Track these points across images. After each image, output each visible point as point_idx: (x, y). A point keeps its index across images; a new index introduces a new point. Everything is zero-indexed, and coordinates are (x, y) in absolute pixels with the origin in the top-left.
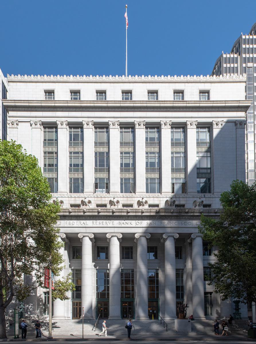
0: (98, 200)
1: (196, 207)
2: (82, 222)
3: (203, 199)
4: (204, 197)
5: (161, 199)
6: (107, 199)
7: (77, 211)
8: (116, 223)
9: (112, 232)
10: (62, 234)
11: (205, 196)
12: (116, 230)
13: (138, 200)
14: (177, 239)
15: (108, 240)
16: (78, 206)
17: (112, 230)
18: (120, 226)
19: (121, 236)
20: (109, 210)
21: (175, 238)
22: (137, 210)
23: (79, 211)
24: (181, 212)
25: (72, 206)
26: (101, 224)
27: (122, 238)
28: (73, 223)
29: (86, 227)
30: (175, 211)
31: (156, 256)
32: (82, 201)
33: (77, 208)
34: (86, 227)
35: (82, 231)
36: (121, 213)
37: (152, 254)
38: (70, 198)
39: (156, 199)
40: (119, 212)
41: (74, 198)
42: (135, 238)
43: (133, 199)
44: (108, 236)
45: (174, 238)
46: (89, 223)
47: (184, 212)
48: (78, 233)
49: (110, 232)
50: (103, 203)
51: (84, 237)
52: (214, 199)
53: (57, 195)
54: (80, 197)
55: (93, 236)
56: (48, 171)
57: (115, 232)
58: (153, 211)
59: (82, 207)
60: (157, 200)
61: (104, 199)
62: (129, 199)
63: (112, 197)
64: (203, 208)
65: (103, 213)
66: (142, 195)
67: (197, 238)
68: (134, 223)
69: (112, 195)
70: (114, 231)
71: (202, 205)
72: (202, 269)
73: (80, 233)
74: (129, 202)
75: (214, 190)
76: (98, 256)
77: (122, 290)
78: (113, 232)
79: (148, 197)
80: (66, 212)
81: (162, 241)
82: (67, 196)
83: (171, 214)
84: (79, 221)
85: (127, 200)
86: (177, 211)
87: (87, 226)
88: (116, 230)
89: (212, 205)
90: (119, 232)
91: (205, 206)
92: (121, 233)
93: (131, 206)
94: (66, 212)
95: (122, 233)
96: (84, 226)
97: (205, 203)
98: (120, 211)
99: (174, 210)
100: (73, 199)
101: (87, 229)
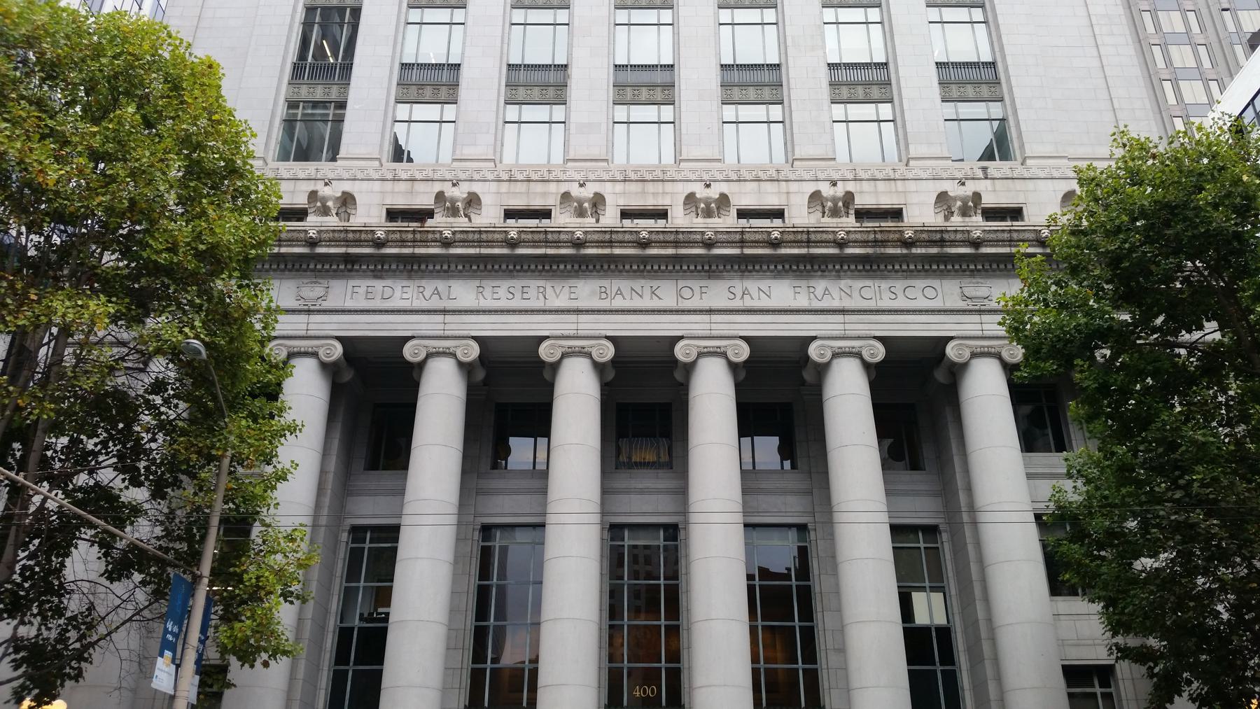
0: (396, 190)
1: (952, 219)
2: (430, 285)
3: (982, 186)
4: (986, 178)
5: (794, 187)
6: (552, 187)
7: (410, 236)
8: (586, 291)
9: (566, 333)
10: (464, 342)
11: (989, 171)
12: (588, 324)
13: (689, 191)
14: (878, 366)
15: (678, 376)
16: (422, 215)
17: (696, 324)
18: (605, 304)
19: (742, 353)
20: (556, 237)
21: (734, 359)
22: (487, 232)
23: (418, 236)
24: (884, 243)
25: (392, 215)
26: (518, 295)
27: (746, 362)
28: (388, 292)
29: (444, 312)
30: (852, 237)
31: (786, 451)
32: (313, 195)
33: (411, 224)
34: (444, 312)
35: (424, 327)
36: (611, 247)
37: (768, 447)
38: (389, 185)
39: (768, 187)
40: (600, 243)
41: (640, 184)
42: (676, 361)
43: (669, 187)
44: (546, 352)
45: (727, 358)
46: (463, 292)
47: (899, 240)
48: (407, 339)
49: (558, 333)
50: (537, 203)
51: (429, 356)
52: (1030, 184)
53: (333, 170)
54: (436, 177)
55: (338, 350)
56: (311, 77)
57: (714, 333)
58: (752, 239)
59: (439, 222)
60: (776, 190)
61: (539, 187)
62: (650, 187)
63: (448, 178)
64: (983, 224)
65: (527, 247)
66: (708, 171)
67: (835, 362)
68: (948, 292)
69: (578, 171)
70: (841, 327)
71: (979, 211)
72: (586, 518)
73: (413, 337)
74: (650, 202)
75: (1022, 146)
76: (501, 452)
77: (809, 636)
78: (572, 333)
79: (735, 178)
80: (361, 241)
81: (940, 376)
82: (490, 177)
83: (905, 251)
84: (417, 282)
85: (876, 192)
86: (865, 237)
87: (450, 305)
88: (721, 324)
89: (904, 210)
90: (597, 333)
91: (992, 214)
92: (607, 338)
93: (662, 214)
94: (361, 241)
95: (746, 339)
96: (435, 303)
97: (989, 200)
98: (607, 237)
99: (848, 233)
100: (402, 186)
101: (449, 318)
